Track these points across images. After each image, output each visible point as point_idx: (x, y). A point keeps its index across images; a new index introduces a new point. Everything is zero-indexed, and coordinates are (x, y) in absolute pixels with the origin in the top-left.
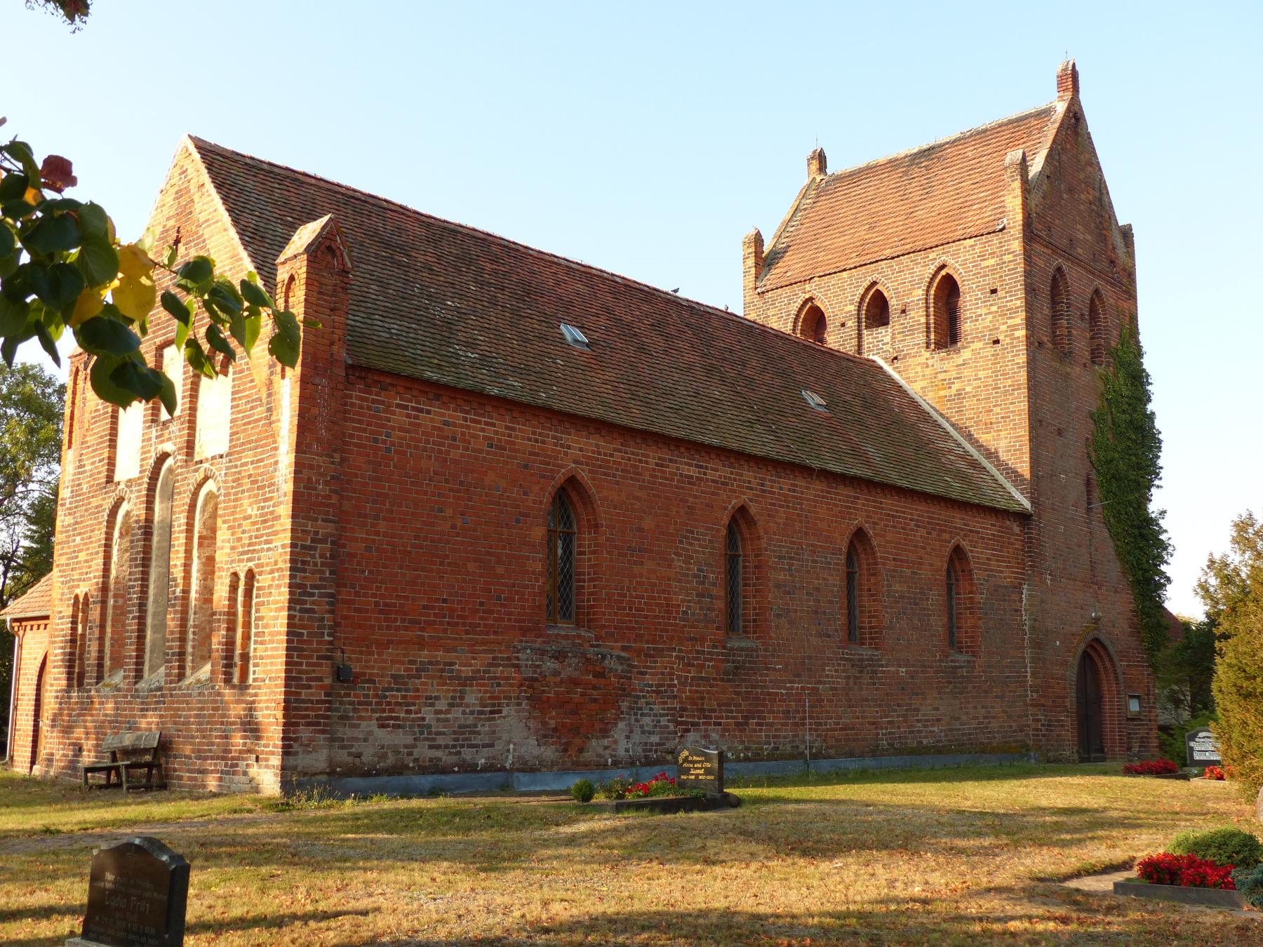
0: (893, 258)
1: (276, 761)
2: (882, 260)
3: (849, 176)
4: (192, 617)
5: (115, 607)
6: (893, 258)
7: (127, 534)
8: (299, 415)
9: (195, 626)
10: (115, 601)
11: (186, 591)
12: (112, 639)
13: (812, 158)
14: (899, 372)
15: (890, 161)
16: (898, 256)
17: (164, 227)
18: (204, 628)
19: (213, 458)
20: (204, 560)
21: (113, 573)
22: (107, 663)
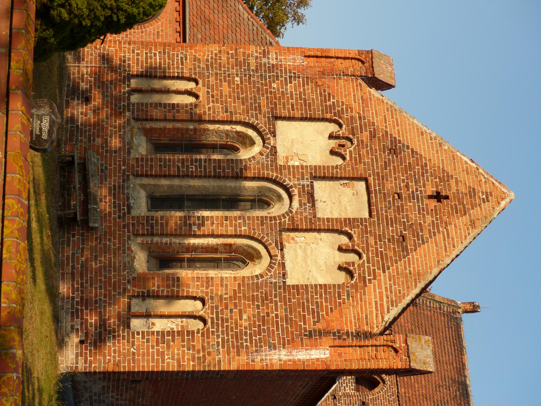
0: (398, 397)
1: (81, 367)
2: (398, 389)
3: (458, 335)
4: (177, 241)
5: (187, 130)
6: (398, 397)
7: (239, 136)
8: (304, 371)
9: (171, 244)
10: (191, 130)
11: (195, 236)
12: (165, 128)
13: (474, 306)
14: (326, 400)
15: (464, 365)
16: (399, 401)
17: (452, 176)
18: (169, 248)
19: (283, 264)
20: (215, 247)
21: (211, 127)
22: (148, 125)
